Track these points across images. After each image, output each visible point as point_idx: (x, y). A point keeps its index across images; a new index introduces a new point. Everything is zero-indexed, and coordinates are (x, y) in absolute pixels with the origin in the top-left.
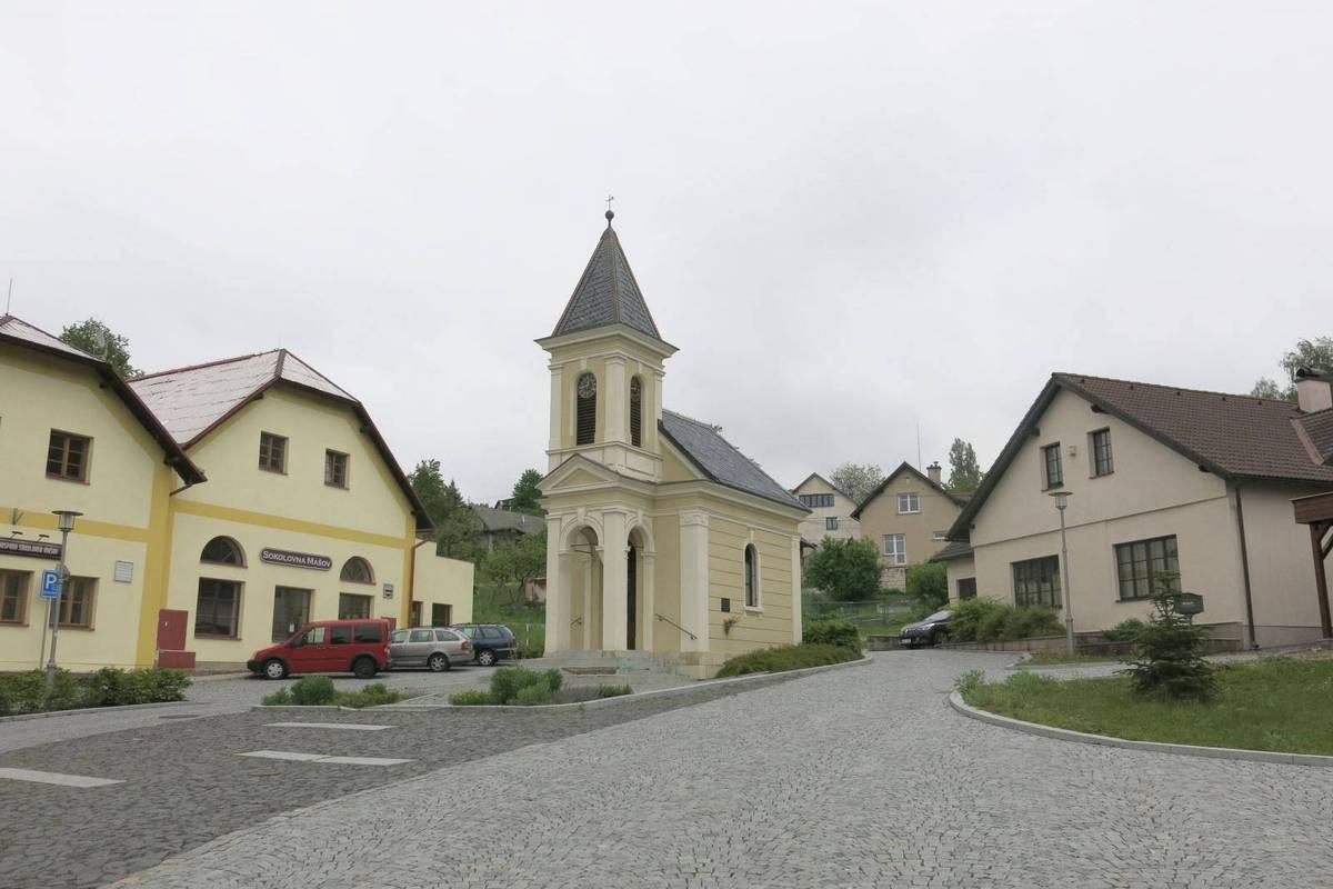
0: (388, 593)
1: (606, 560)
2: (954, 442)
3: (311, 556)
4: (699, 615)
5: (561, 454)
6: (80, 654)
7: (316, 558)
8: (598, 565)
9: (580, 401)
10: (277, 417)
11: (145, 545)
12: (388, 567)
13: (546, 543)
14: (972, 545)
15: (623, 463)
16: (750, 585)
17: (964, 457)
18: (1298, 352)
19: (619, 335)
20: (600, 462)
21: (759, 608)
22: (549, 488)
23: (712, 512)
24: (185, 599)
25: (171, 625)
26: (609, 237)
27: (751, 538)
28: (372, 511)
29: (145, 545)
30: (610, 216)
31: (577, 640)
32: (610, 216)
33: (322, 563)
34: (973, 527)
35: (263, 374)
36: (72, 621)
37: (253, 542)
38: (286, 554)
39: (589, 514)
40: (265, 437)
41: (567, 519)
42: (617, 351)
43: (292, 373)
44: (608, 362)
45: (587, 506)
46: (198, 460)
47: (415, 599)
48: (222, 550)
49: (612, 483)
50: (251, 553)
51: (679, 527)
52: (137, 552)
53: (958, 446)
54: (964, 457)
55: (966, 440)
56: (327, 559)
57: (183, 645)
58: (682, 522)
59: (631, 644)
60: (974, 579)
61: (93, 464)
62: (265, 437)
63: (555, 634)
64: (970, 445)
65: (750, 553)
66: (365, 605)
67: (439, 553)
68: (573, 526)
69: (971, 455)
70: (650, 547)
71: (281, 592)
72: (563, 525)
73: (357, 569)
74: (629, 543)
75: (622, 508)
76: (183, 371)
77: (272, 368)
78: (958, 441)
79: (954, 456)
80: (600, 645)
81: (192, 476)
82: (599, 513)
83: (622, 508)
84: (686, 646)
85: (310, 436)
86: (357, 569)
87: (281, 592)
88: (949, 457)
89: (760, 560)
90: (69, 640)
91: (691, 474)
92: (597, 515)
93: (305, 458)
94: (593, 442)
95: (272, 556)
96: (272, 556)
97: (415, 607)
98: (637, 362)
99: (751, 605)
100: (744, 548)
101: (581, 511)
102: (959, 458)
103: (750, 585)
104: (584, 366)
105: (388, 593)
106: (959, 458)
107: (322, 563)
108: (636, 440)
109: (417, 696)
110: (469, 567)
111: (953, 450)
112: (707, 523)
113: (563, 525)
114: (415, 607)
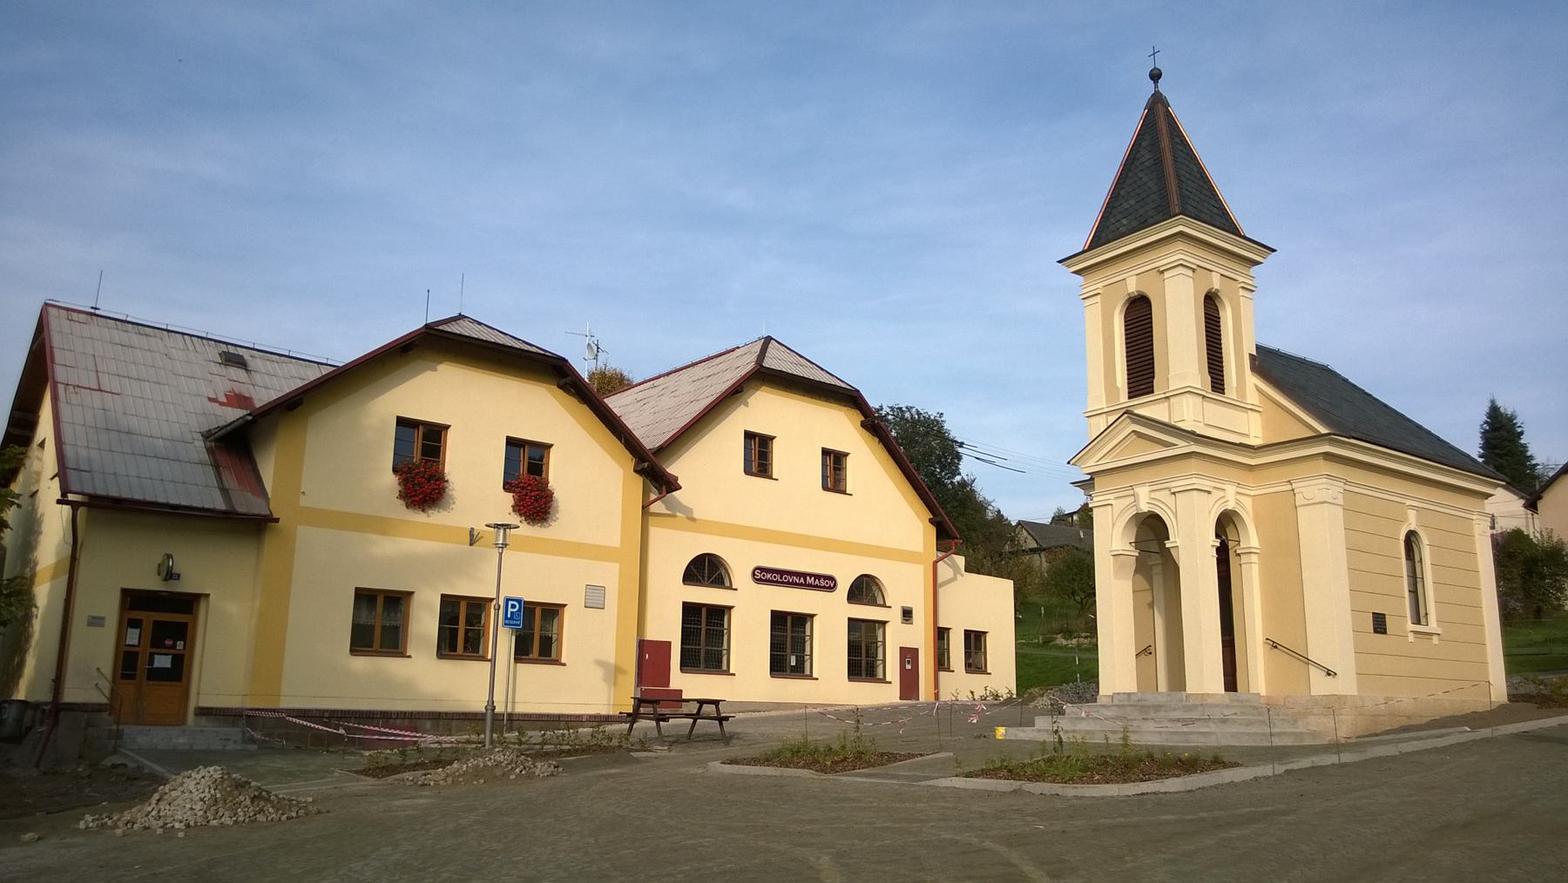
0: (907, 614)
3: (811, 575)
4: (1332, 632)
6: (538, 691)
7: (818, 577)
8: (1171, 568)
10: (766, 411)
11: (617, 566)
12: (904, 585)
19: (1181, 234)
21: (1433, 625)
23: (1346, 482)
24: (667, 627)
25: (651, 657)
27: (1412, 523)
28: (882, 516)
29: (617, 566)
30: (1155, 76)
31: (1145, 676)
32: (1155, 76)
33: (825, 583)
35: (746, 364)
36: (465, 648)
37: (740, 560)
38: (782, 572)
40: (749, 436)
43: (774, 361)
44: (1167, 275)
46: (673, 469)
47: (941, 625)
48: (706, 569)
49: (1183, 447)
50: (740, 573)
52: (609, 576)
55: (1506, 406)
56: (832, 578)
57: (666, 679)
58: (1299, 500)
59: (1231, 683)
61: (921, 578)
62: (749, 436)
63: (1117, 668)
65: (1411, 539)
66: (808, 626)
67: (969, 568)
68: (1133, 512)
70: (1250, 538)
71: (778, 618)
73: (864, 589)
74: (1217, 536)
75: (1206, 484)
76: (668, 374)
77: (753, 358)
81: (668, 485)
83: (1206, 484)
84: (1320, 686)
85: (802, 429)
86: (864, 589)
87: (778, 618)
89: (1426, 553)
90: (532, 674)
91: (1314, 430)
93: (797, 460)
95: (765, 576)
96: (765, 576)
97: (941, 634)
99: (1419, 623)
100: (1402, 537)
104: (1132, 287)
105: (907, 614)
107: (825, 583)
108: (1218, 384)
109: (892, 758)
110: (1007, 586)
112: (1340, 501)
114: (941, 634)
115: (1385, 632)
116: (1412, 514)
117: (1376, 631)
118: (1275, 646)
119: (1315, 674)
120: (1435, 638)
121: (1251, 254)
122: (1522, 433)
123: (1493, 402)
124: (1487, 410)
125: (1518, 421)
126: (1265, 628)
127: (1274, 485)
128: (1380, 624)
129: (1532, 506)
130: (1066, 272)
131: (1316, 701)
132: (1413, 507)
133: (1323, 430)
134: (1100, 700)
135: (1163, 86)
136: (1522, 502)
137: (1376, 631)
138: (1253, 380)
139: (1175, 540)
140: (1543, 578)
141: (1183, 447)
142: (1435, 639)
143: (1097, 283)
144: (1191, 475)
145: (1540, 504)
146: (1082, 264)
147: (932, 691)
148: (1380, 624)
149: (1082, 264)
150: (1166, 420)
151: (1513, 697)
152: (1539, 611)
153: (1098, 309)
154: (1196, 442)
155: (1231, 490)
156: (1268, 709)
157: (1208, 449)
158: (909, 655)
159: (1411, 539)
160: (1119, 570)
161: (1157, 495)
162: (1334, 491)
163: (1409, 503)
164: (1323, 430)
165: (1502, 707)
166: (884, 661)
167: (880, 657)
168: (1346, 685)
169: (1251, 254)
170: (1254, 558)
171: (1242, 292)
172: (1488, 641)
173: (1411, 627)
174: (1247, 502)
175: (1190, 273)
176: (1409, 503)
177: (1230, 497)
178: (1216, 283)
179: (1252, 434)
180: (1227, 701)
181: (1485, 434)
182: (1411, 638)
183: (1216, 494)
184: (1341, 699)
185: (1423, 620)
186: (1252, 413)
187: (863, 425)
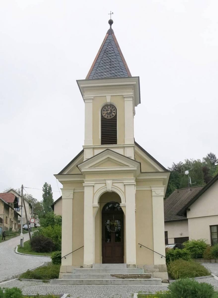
2: (44, 183)
5: (93, 148)
9: (104, 120)
14: (188, 217)
17: (48, 189)
20: (123, 154)
22: (87, 167)
26: (110, 32)
30: (111, 22)
32: (111, 22)
34: (189, 210)
39: (114, 184)
41: (97, 187)
44: (125, 99)
45: (113, 180)
51: (152, 196)
53: (46, 185)
54: (48, 189)
55: (49, 183)
58: (154, 194)
64: (50, 185)
69: (50, 189)
72: (95, 190)
78: (46, 183)
79: (44, 188)
80: (154, 264)
88: (43, 189)
91: (154, 168)
92: (121, 186)
94: (116, 143)
101: (109, 182)
102: (46, 189)
104: (109, 100)
106: (46, 189)
111: (44, 186)
113: (95, 190)
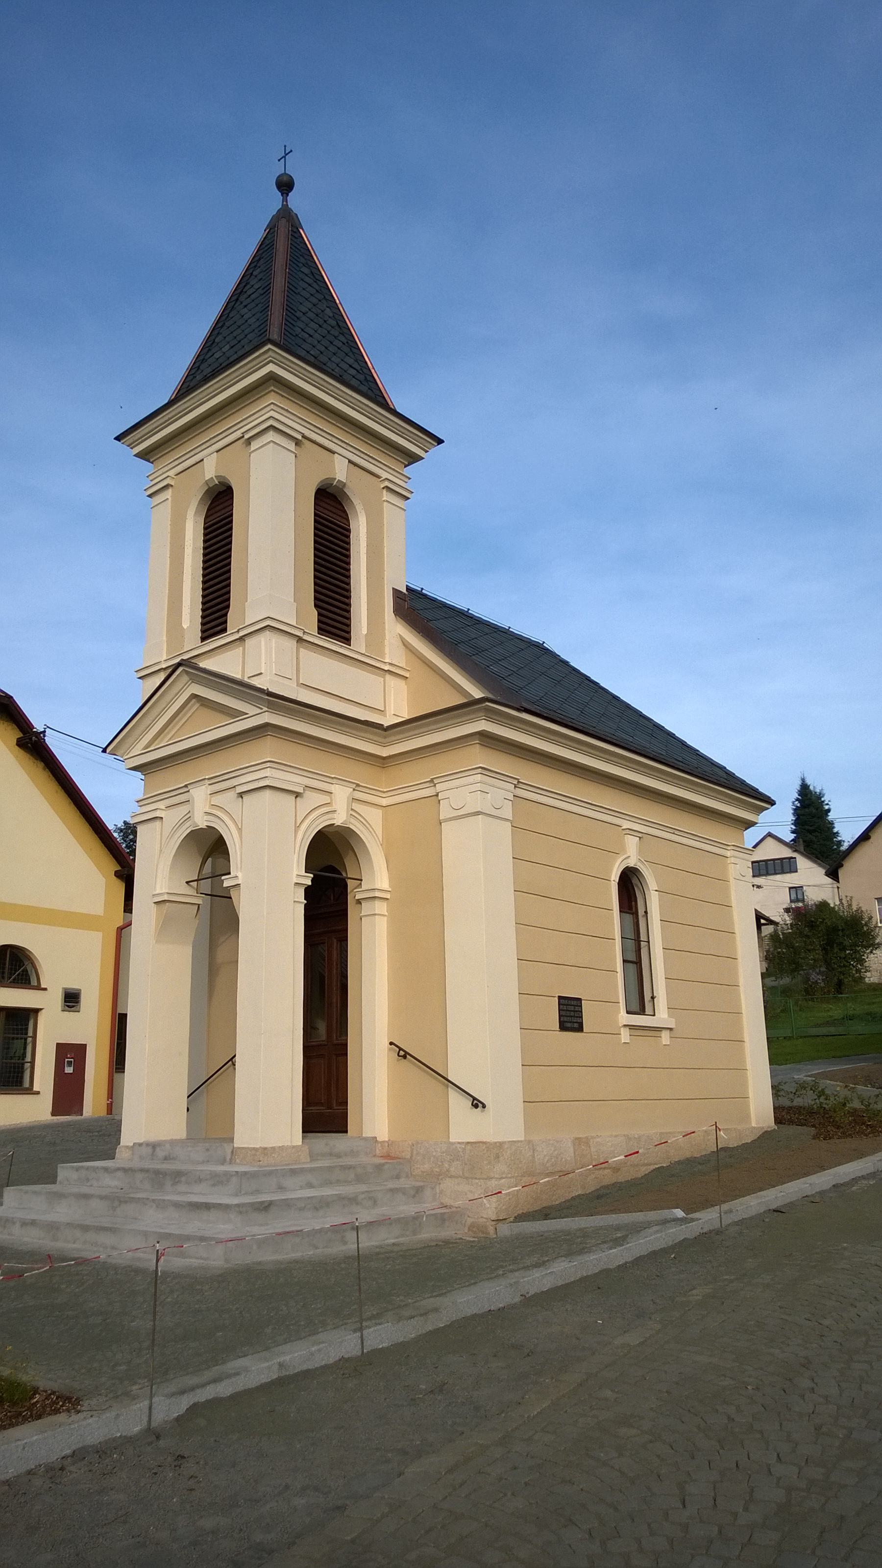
0: (71, 999)
1: (247, 907)
4: (486, 1033)
13: (773, 1087)
15: (291, 673)
16: (635, 960)
18: (835, 830)
21: (662, 1016)
27: (631, 855)
30: (285, 185)
32: (285, 185)
42: (271, 367)
44: (255, 445)
49: (256, 716)
55: (815, 785)
58: (445, 812)
60: (126, 1015)
65: (629, 882)
70: (375, 874)
75: (293, 781)
82: (232, 794)
84: (464, 1127)
89: (653, 903)
98: (334, 453)
99: (642, 1011)
100: (615, 877)
103: (635, 960)
104: (210, 470)
105: (71, 999)
115: (580, 1029)
116: (632, 843)
117: (563, 1027)
118: (404, 1055)
119: (458, 1104)
120: (665, 1035)
121: (408, 443)
122: (829, 810)
123: (803, 780)
124: (800, 783)
125: (826, 799)
126: (390, 1025)
127: (409, 785)
128: (570, 1015)
129: (833, 874)
130: (126, 453)
131: (455, 1152)
132: (634, 835)
133: (477, 693)
134: (122, 1156)
135: (295, 200)
136: (823, 871)
137: (563, 1027)
138: (396, 630)
139: (240, 871)
140: (844, 949)
141: (256, 716)
142: (665, 1038)
143: (168, 469)
144: (263, 763)
145: (841, 873)
146: (152, 439)
147: (104, 1101)
148: (570, 1015)
149: (152, 439)
150: (238, 676)
151: (782, 1114)
152: (840, 984)
153: (167, 508)
154: (272, 707)
155: (341, 794)
156: (391, 1162)
157: (294, 722)
158: (71, 1055)
159: (629, 882)
160: (165, 927)
161: (218, 800)
162: (497, 796)
163: (626, 825)
164: (477, 693)
165: (766, 1135)
166: (33, 1063)
167: (28, 1058)
168: (503, 1123)
169: (408, 443)
170: (381, 908)
171: (386, 495)
172: (746, 1038)
173: (624, 1018)
174: (374, 817)
175: (292, 446)
176: (626, 825)
177: (338, 806)
178: (340, 471)
179: (391, 710)
180: (304, 1160)
181: (796, 811)
182: (625, 1036)
183: (312, 799)
184: (495, 1150)
185: (648, 1010)
186: (388, 675)
187: (20, 744)
